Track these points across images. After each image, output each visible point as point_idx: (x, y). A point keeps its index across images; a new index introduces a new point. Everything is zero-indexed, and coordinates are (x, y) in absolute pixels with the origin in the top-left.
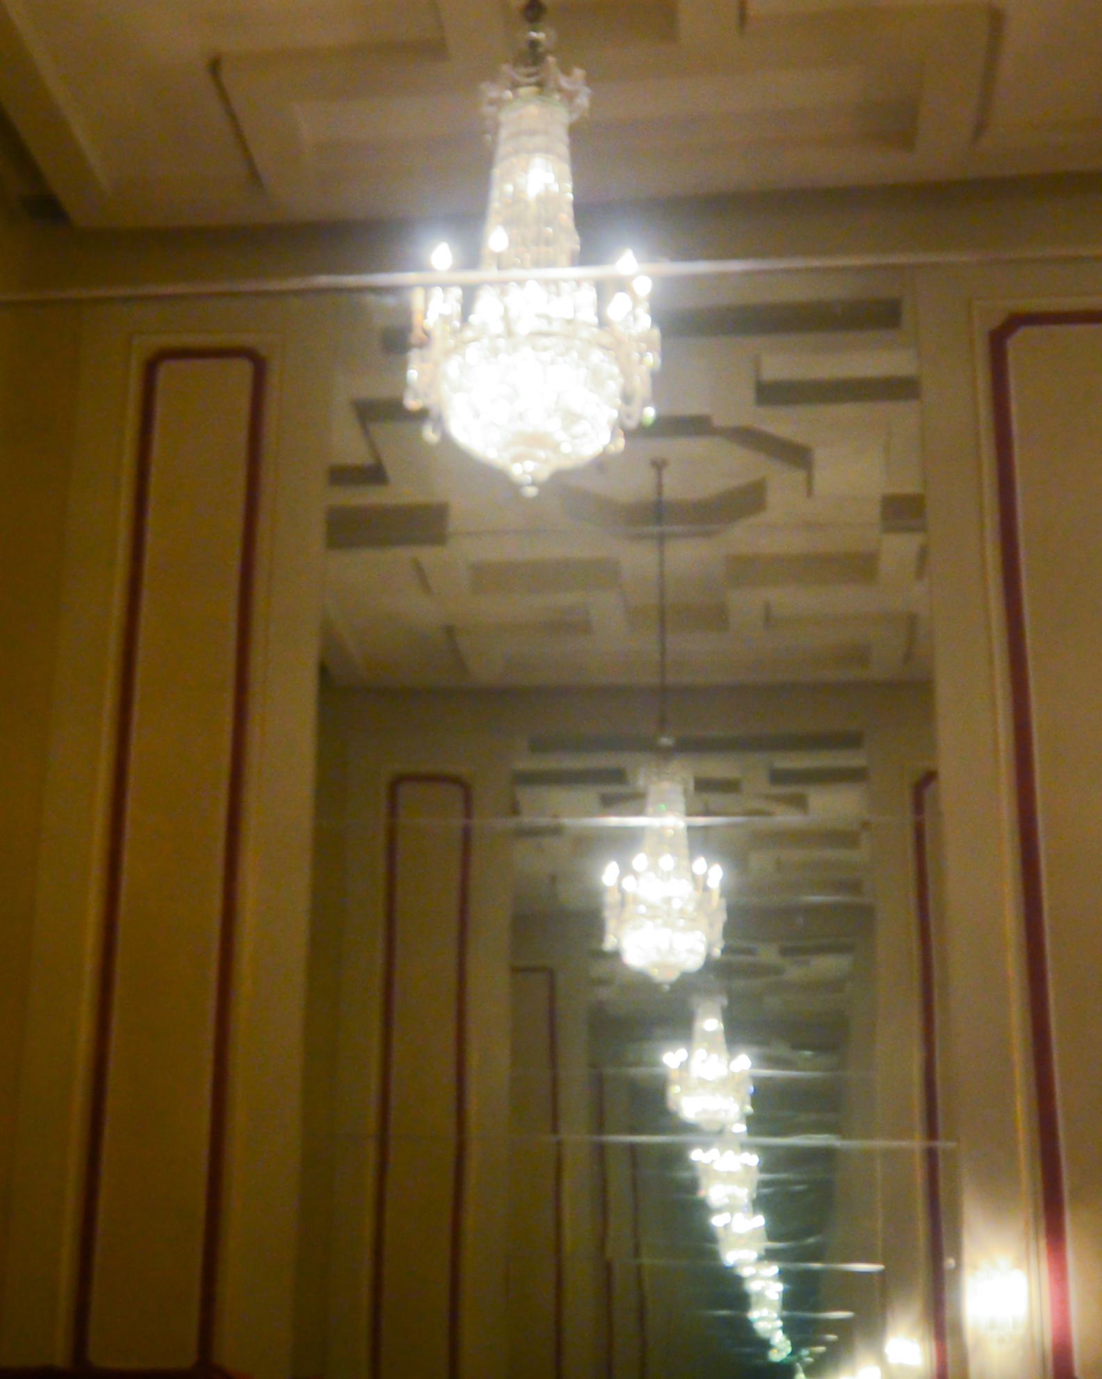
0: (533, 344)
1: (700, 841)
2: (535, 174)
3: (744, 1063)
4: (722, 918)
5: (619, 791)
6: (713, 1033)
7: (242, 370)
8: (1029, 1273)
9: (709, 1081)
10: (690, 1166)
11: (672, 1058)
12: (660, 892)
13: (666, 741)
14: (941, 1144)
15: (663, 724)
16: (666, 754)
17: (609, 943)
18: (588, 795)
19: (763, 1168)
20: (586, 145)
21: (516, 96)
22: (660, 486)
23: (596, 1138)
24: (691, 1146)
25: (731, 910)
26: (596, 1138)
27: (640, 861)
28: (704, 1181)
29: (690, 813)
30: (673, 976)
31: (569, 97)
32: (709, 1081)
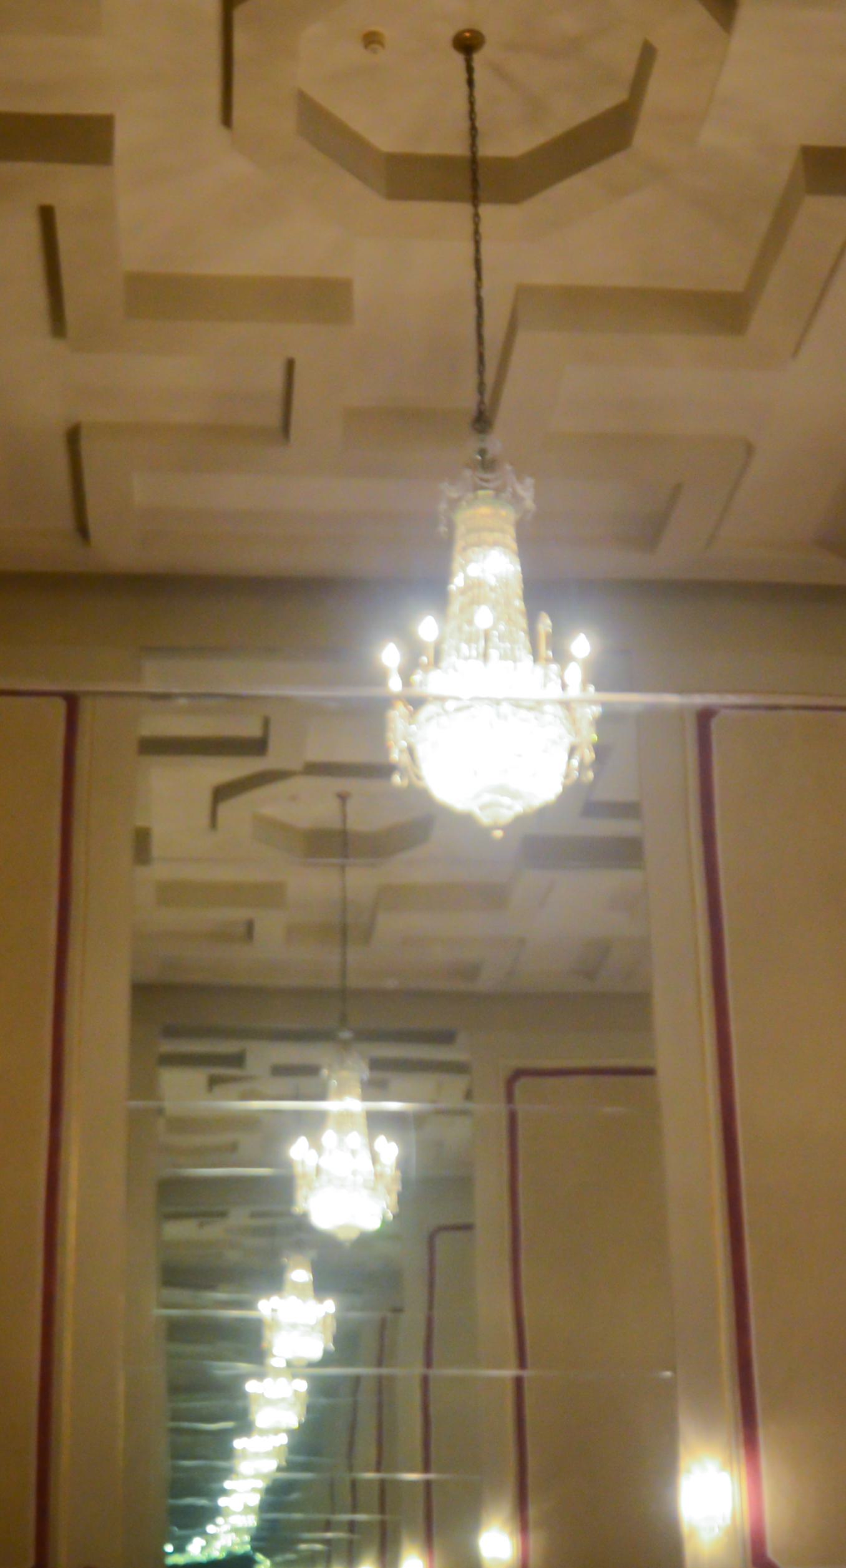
0: (491, 710)
1: (376, 1122)
2: (489, 566)
3: (330, 1306)
4: (397, 1187)
5: (303, 1078)
6: (304, 1284)
7: (60, 707)
8: (732, 1471)
9: (297, 1322)
10: (245, 1395)
11: (266, 1307)
12: (347, 1165)
13: (346, 1035)
14: (434, 1372)
15: (343, 1020)
16: (346, 1045)
17: (298, 1209)
18: (197, 1077)
19: (311, 1392)
20: (530, 543)
21: (476, 498)
22: (344, 817)
23: (384, 1371)
24: (245, 1377)
25: (405, 1182)
26: (384, 1371)
27: (329, 1137)
28: (253, 1408)
29: (365, 1098)
30: (353, 1235)
31: (516, 500)
32: (297, 1322)
